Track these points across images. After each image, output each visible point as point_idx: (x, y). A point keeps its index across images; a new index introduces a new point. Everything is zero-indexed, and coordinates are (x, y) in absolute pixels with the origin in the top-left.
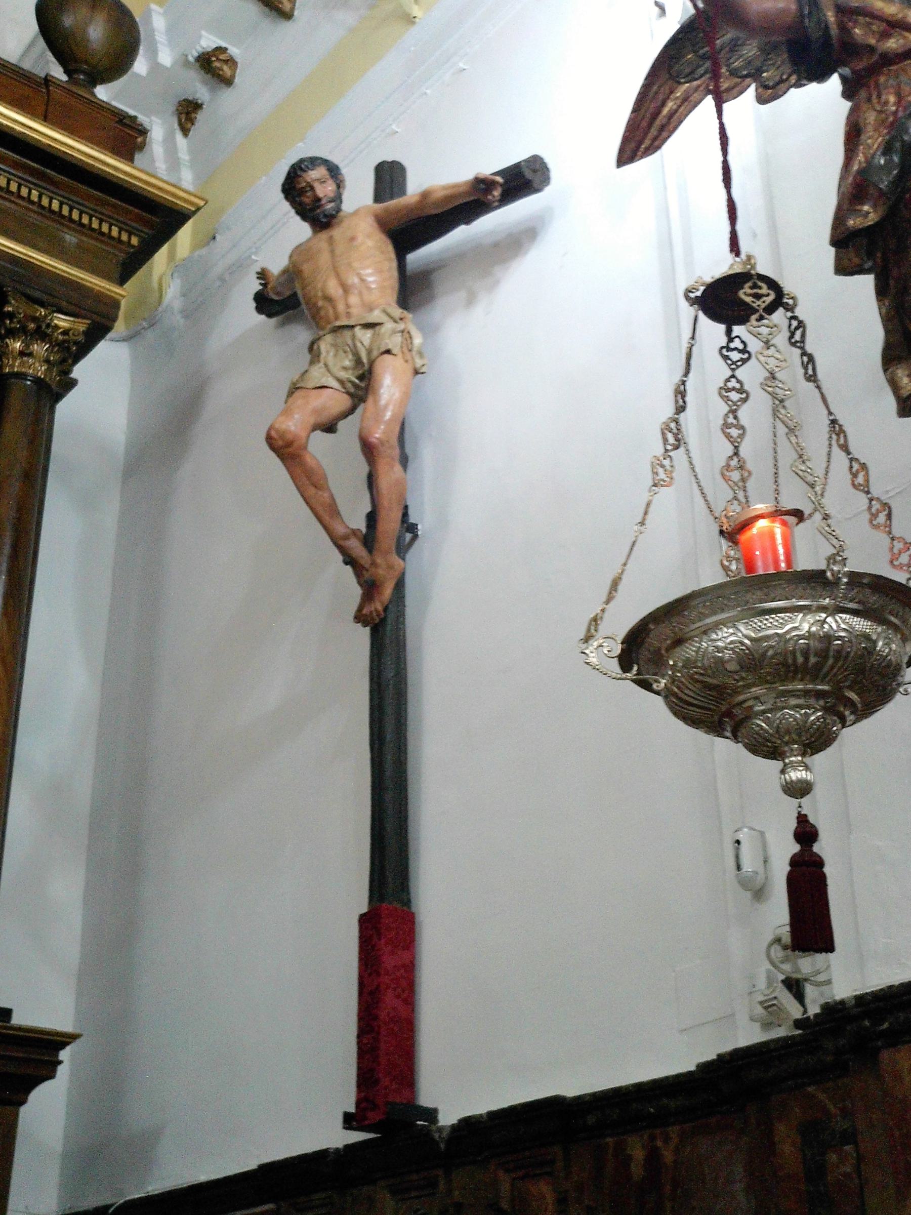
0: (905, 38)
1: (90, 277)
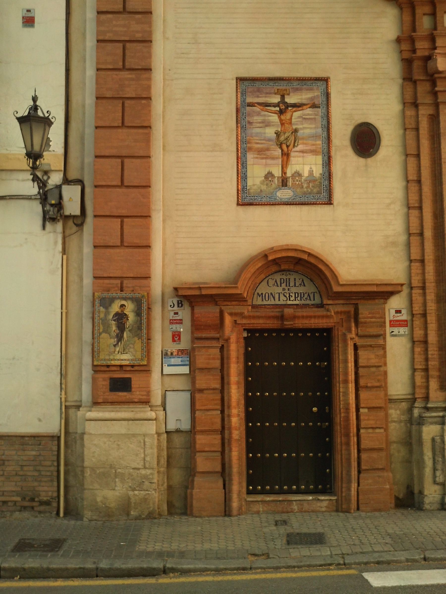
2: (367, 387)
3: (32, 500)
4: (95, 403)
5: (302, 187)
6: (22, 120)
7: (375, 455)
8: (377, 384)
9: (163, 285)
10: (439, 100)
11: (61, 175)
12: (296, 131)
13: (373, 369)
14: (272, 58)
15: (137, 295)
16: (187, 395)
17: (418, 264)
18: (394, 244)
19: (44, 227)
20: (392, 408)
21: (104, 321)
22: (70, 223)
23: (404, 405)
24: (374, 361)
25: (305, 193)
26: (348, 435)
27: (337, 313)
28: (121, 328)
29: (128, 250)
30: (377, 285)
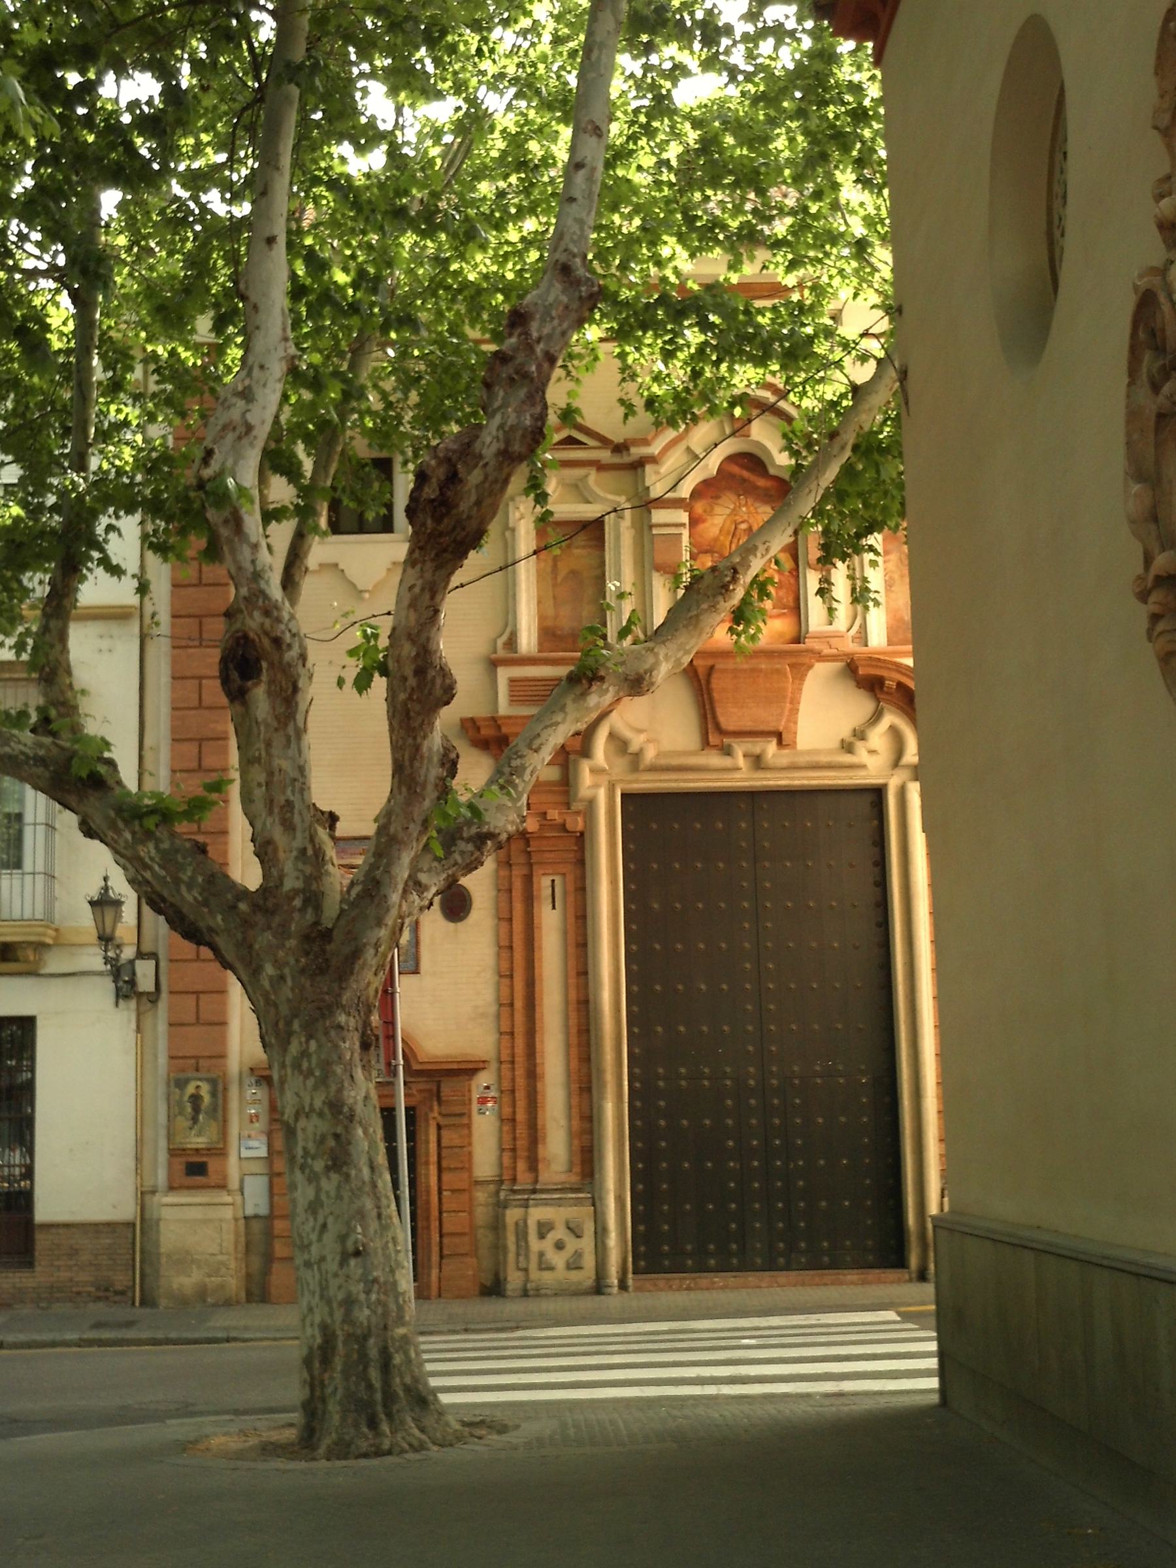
3: (107, 1290)
4: (171, 1188)
6: (92, 903)
7: (457, 1240)
8: (460, 1165)
9: (241, 1062)
11: (135, 949)
13: (457, 1150)
15: (213, 1075)
16: (265, 1179)
17: (507, 1037)
18: (483, 1015)
19: (117, 1005)
21: (180, 1103)
22: (144, 999)
23: (492, 1187)
24: (457, 1142)
26: (428, 1219)
27: (420, 1091)
28: (196, 1109)
29: (204, 1028)
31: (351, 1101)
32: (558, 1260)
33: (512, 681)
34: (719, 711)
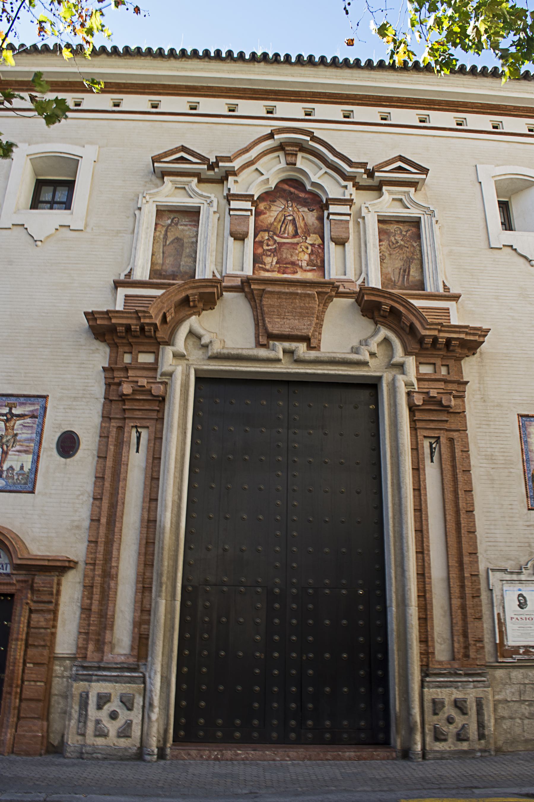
0: (117, 742)
1: (176, 458)
2: (34, 645)
5: (13, 479)
8: (42, 643)
10: (129, 375)
12: (16, 435)
14: (7, 380)
18: (78, 527)
20: (57, 665)
25: (14, 484)
27: (18, 581)
30: (49, 560)
31: (172, 229)
32: (112, 727)
33: (420, 217)
34: (267, 320)
